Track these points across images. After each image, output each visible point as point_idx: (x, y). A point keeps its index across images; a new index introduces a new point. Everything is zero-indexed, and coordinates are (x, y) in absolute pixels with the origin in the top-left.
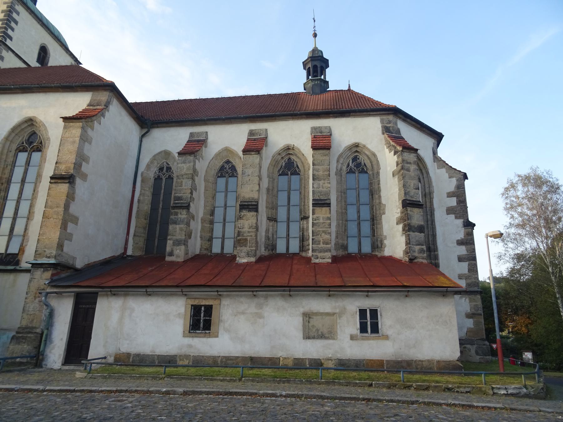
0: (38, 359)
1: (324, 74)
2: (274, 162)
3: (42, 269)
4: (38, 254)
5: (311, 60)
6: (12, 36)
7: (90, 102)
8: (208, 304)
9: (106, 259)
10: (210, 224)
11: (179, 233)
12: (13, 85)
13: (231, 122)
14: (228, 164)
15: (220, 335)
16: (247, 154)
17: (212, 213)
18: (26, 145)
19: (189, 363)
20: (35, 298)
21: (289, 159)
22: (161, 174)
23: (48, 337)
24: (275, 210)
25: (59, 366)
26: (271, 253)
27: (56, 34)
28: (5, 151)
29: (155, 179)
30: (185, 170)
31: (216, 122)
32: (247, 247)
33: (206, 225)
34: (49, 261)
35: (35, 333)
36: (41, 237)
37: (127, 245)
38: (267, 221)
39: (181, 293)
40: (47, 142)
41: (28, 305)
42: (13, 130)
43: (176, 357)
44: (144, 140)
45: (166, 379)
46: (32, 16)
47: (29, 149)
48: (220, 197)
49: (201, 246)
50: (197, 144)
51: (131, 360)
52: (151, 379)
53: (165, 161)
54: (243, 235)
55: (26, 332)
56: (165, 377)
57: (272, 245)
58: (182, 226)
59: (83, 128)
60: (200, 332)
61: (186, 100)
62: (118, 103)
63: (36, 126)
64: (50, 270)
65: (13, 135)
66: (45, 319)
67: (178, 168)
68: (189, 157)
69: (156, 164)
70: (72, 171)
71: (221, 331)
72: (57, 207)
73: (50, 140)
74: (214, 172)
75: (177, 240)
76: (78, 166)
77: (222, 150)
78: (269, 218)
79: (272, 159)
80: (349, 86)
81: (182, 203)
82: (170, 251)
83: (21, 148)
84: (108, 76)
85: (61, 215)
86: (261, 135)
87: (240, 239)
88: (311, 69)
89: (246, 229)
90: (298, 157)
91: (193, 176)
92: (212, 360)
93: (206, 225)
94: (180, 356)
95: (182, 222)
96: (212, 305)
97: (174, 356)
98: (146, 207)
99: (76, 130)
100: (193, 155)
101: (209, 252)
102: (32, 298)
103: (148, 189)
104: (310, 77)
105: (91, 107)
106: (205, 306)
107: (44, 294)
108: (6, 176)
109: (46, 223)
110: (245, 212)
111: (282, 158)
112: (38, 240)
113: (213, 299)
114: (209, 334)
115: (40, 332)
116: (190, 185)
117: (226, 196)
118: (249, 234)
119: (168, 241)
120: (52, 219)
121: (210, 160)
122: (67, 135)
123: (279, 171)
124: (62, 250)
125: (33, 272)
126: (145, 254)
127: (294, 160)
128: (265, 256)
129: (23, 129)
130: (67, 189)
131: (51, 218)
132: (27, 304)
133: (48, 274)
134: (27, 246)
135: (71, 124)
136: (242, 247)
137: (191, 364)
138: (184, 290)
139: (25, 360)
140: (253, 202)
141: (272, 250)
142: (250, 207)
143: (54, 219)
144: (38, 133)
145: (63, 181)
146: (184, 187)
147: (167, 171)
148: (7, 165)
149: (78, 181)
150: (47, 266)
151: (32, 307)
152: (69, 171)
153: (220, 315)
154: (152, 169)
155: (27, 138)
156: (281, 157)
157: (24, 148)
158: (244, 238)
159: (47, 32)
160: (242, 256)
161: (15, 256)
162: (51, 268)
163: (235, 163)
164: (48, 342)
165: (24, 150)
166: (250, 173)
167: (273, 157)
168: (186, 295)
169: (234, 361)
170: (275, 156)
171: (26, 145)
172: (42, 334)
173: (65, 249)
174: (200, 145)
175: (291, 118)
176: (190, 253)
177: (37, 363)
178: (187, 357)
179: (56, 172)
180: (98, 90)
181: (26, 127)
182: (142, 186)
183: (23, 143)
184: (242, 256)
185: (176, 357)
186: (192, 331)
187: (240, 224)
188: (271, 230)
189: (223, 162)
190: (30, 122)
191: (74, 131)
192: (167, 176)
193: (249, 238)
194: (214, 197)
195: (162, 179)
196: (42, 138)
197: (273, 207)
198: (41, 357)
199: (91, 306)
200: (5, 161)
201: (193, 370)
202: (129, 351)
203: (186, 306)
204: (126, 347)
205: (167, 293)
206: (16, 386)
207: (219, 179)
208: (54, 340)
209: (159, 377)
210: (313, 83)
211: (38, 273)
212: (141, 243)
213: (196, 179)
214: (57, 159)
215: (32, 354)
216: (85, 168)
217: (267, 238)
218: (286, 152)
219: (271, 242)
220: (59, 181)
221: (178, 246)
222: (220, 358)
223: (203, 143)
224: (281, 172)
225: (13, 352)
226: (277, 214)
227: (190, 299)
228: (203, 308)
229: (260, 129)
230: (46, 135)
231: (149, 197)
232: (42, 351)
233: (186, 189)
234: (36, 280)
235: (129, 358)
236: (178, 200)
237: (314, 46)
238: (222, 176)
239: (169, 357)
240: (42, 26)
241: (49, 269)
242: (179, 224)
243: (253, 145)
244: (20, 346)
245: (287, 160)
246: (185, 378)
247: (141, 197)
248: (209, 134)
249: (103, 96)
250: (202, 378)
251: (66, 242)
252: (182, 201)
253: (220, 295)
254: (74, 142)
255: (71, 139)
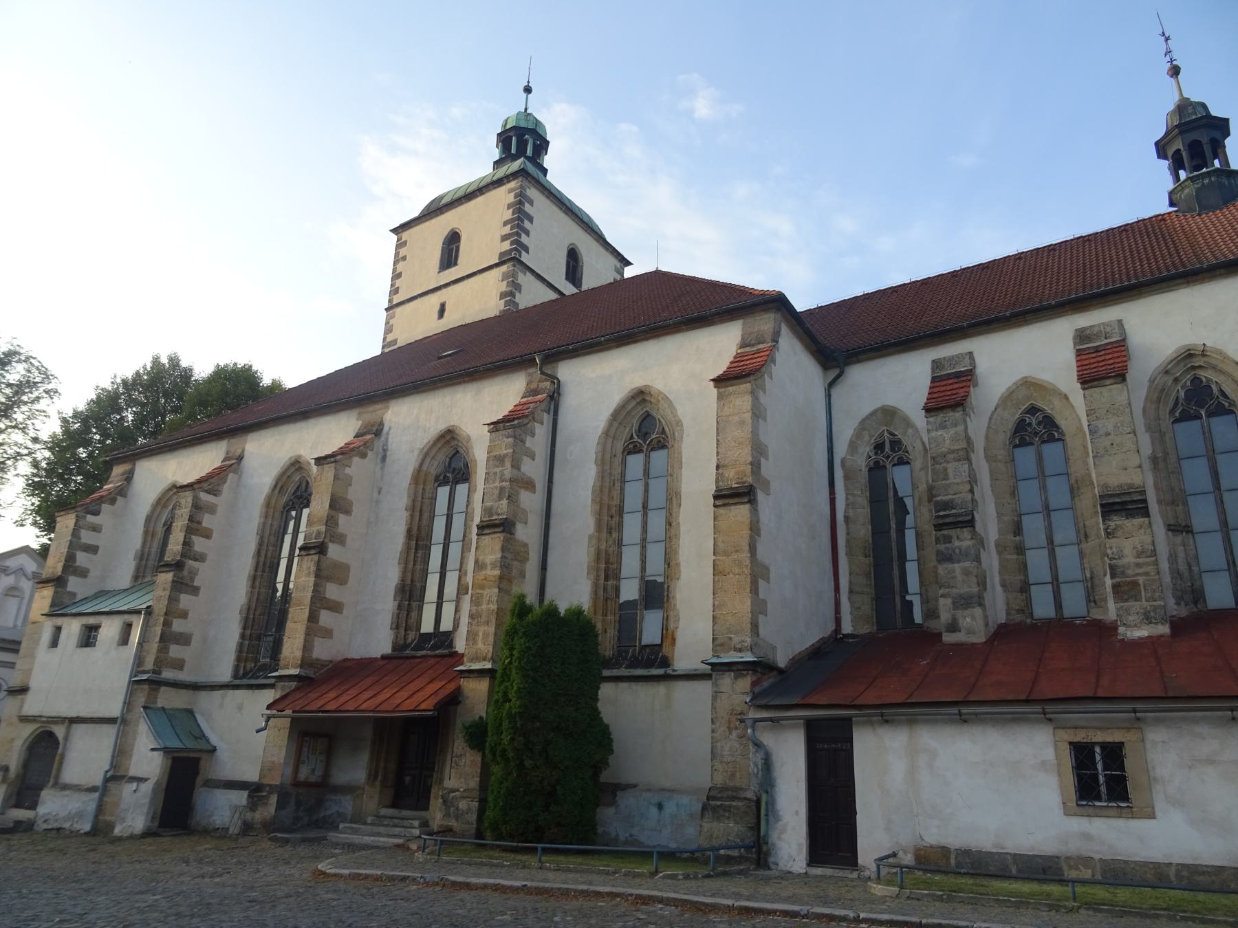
0: (759, 852)
1: (1221, 155)
2: (1157, 394)
3: (732, 674)
4: (719, 645)
5: (1181, 133)
6: (528, 245)
7: (743, 339)
8: (1111, 740)
9: (813, 645)
10: (1018, 554)
11: (963, 581)
12: (603, 336)
13: (1026, 321)
14: (1033, 415)
15: (1158, 813)
16: (1092, 387)
17: (1018, 529)
18: (639, 441)
19: (1093, 876)
20: (730, 729)
21: (1196, 379)
22: (880, 457)
23: (770, 807)
24: (1181, 507)
25: (801, 868)
26: (1196, 610)
27: (586, 220)
28: (608, 456)
29: (870, 470)
30: (948, 442)
31: (991, 327)
32: (1139, 600)
33: (1009, 557)
34: (742, 658)
35: (745, 799)
36: (717, 612)
37: (840, 614)
38: (1167, 534)
39: (1042, 716)
40: (679, 428)
41: (719, 744)
42: (615, 415)
43: (1056, 860)
44: (835, 392)
45: (1082, 911)
46: (552, 201)
47: (645, 447)
48: (1030, 494)
49: (1008, 604)
50: (956, 383)
51: (953, 862)
52: (1047, 909)
53: (885, 428)
54: (1123, 573)
55: (727, 797)
56: (1079, 908)
57: (1193, 591)
58: (967, 564)
59: (752, 392)
60: (1105, 804)
61: (880, 291)
62: (788, 331)
63: (651, 402)
64: (748, 674)
65: (616, 424)
66: (756, 771)
67: (932, 441)
68: (952, 414)
69: (866, 438)
70: (750, 480)
71: (1160, 806)
72: (737, 551)
73: (682, 425)
74: (1003, 437)
75: (961, 596)
76: (756, 466)
77: (1015, 387)
78: (1172, 528)
79: (1150, 387)
80: (528, 82)
81: (955, 515)
82: (950, 621)
83: (631, 446)
84: (757, 280)
85: (747, 566)
86: (1110, 337)
87: (1119, 583)
88: (1184, 154)
89: (1129, 558)
90: (1221, 372)
91: (967, 453)
92: (1152, 872)
93: (1009, 557)
94: (1068, 858)
95: (964, 555)
96: (1123, 743)
97: (1052, 857)
98: (864, 531)
99: (741, 399)
100: (960, 408)
101: (1027, 618)
102: (724, 731)
103: (860, 493)
104: (1183, 175)
105: (747, 349)
106: (1104, 746)
107: (749, 723)
108: (616, 501)
109: (722, 585)
110: (1116, 521)
111: (1176, 380)
112: (714, 617)
113: (1123, 728)
114: (1129, 810)
115: (755, 799)
116: (967, 474)
117: (1044, 487)
118: (1140, 571)
119: (942, 601)
120: (731, 575)
121: (990, 413)
122: (727, 411)
123: (1172, 411)
124: (758, 635)
125: (716, 680)
126: (878, 630)
127: (1208, 380)
128: (1180, 618)
129: (629, 412)
130: (749, 515)
131: (729, 573)
132: (717, 742)
133: (745, 683)
134: (678, 630)
135: (730, 389)
136: (1127, 600)
137: (1099, 877)
138: (1049, 708)
139: (735, 853)
140: (1133, 495)
141: (1196, 603)
142: (1130, 507)
143: (735, 575)
144: (655, 415)
145: (736, 500)
146: (952, 480)
147: (892, 449)
148: (614, 481)
149: (760, 496)
150: (740, 667)
151: (727, 748)
152: (744, 479)
153: (1150, 766)
154: (861, 450)
155: (637, 428)
156: (1172, 378)
157: (635, 446)
158: (1128, 579)
159: (574, 220)
160: (1132, 624)
161: (656, 648)
162: (748, 670)
163: (1052, 409)
164: (771, 818)
165: (636, 450)
166: (1110, 428)
167: (1152, 381)
168: (1050, 720)
169: (1214, 878)
170: (1155, 378)
171: (639, 441)
172: (758, 802)
173: (762, 632)
174: (965, 384)
175: (1183, 283)
176: (991, 624)
177: (759, 858)
178: (1086, 861)
179: (721, 484)
180: (753, 313)
181: (633, 408)
182: (847, 488)
183: (632, 437)
184: (1132, 624)
185: (1056, 860)
186: (1084, 803)
187: (1111, 548)
188: (1181, 555)
189: (1020, 411)
190: (641, 396)
191: (738, 402)
192: (896, 459)
193: (1141, 580)
194: (1014, 492)
195: (884, 467)
196: (664, 423)
197: (1176, 498)
198: (765, 848)
199: (840, 745)
200: (610, 474)
201: (1101, 893)
202: (944, 841)
203: (1055, 744)
204: (934, 836)
205: (1003, 716)
206: (801, 907)
207: (1018, 452)
208: (781, 813)
209: (1065, 907)
210: (1196, 186)
211: (726, 681)
212: (867, 608)
213: (973, 456)
214: (718, 459)
215: (747, 842)
216: (767, 469)
217: (1176, 574)
218: (1182, 364)
219: (1189, 584)
220: (731, 501)
221: (966, 609)
222: (1173, 870)
223: (969, 378)
224: (1177, 414)
225: (711, 836)
226: (1187, 513)
227: (1063, 728)
228: (1098, 750)
229: (1103, 323)
230: (674, 416)
231: (864, 508)
232: (765, 836)
233: (958, 484)
234: (724, 696)
235: (948, 859)
236: (944, 510)
237: (1177, 98)
238: (1023, 443)
239: (1040, 861)
240: (566, 214)
241: (745, 672)
242: (959, 562)
243: (1098, 362)
244: (721, 824)
245: (1188, 383)
246: (1130, 912)
247: (850, 510)
248: (976, 355)
249: (766, 322)
250: (1175, 915)
251: (761, 618)
252: (954, 511)
253: (1138, 719)
254: (742, 423)
255: (736, 418)
